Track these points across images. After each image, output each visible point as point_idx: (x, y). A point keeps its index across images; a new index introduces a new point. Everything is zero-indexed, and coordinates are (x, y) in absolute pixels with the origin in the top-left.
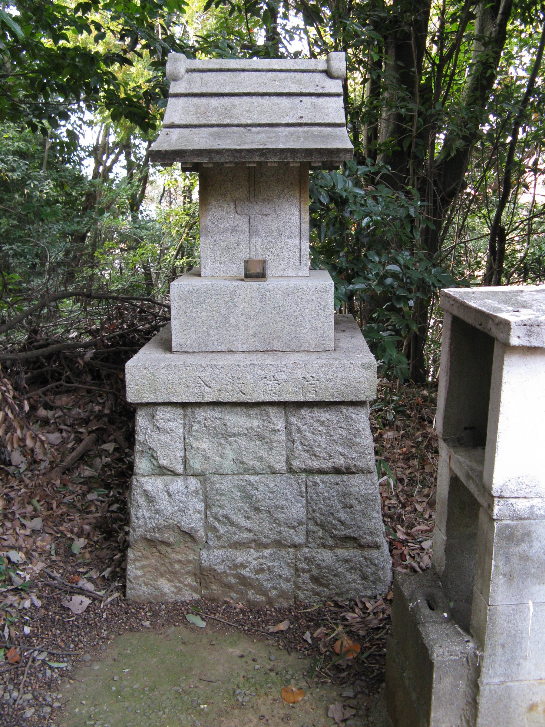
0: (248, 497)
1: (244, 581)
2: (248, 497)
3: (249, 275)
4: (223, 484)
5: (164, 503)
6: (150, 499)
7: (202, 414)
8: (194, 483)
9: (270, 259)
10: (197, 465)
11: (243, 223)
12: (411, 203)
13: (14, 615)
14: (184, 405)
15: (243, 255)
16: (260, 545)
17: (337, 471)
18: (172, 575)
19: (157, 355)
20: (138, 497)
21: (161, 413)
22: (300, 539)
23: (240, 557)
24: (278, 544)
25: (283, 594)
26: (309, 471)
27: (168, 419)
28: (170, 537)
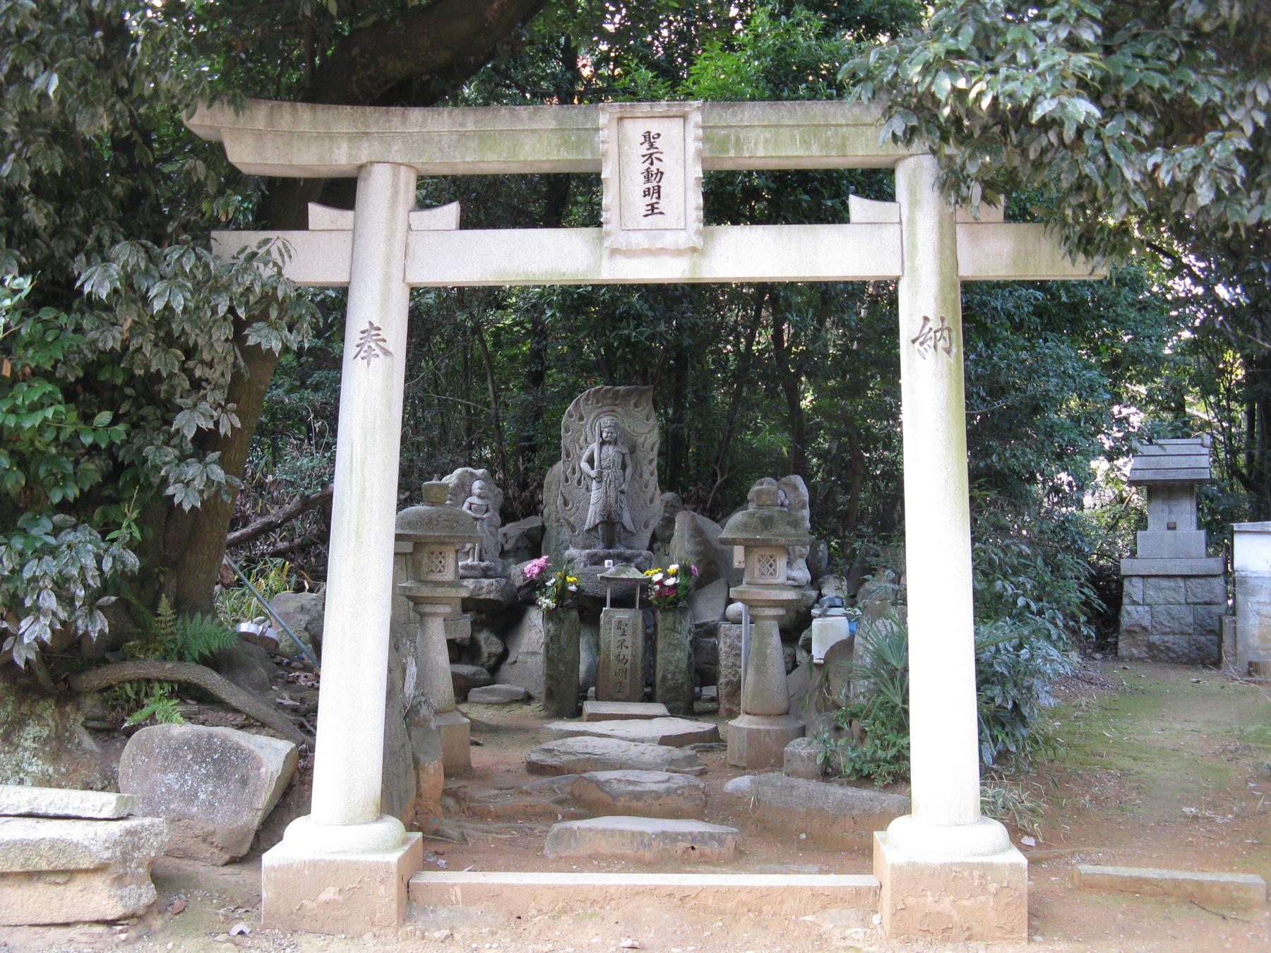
0: (1169, 614)
1: (1168, 649)
2: (1169, 614)
3: (1169, 528)
4: (1159, 608)
5: (1135, 615)
6: (1129, 613)
7: (1150, 580)
8: (1147, 608)
9: (1178, 524)
10: (1148, 600)
11: (1166, 508)
12: (440, 848)
13: (1044, 142)
14: (1143, 577)
15: (1166, 520)
16: (1174, 634)
17: (1206, 603)
18: (1137, 646)
19: (519, 711)
20: (1124, 613)
21: (1134, 579)
22: (1191, 631)
23: (1166, 638)
24: (1182, 633)
25: (1184, 654)
26: (1195, 604)
27: (1012, 567)
28: (1137, 629)
